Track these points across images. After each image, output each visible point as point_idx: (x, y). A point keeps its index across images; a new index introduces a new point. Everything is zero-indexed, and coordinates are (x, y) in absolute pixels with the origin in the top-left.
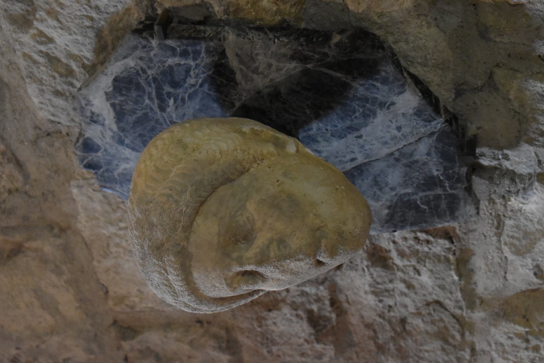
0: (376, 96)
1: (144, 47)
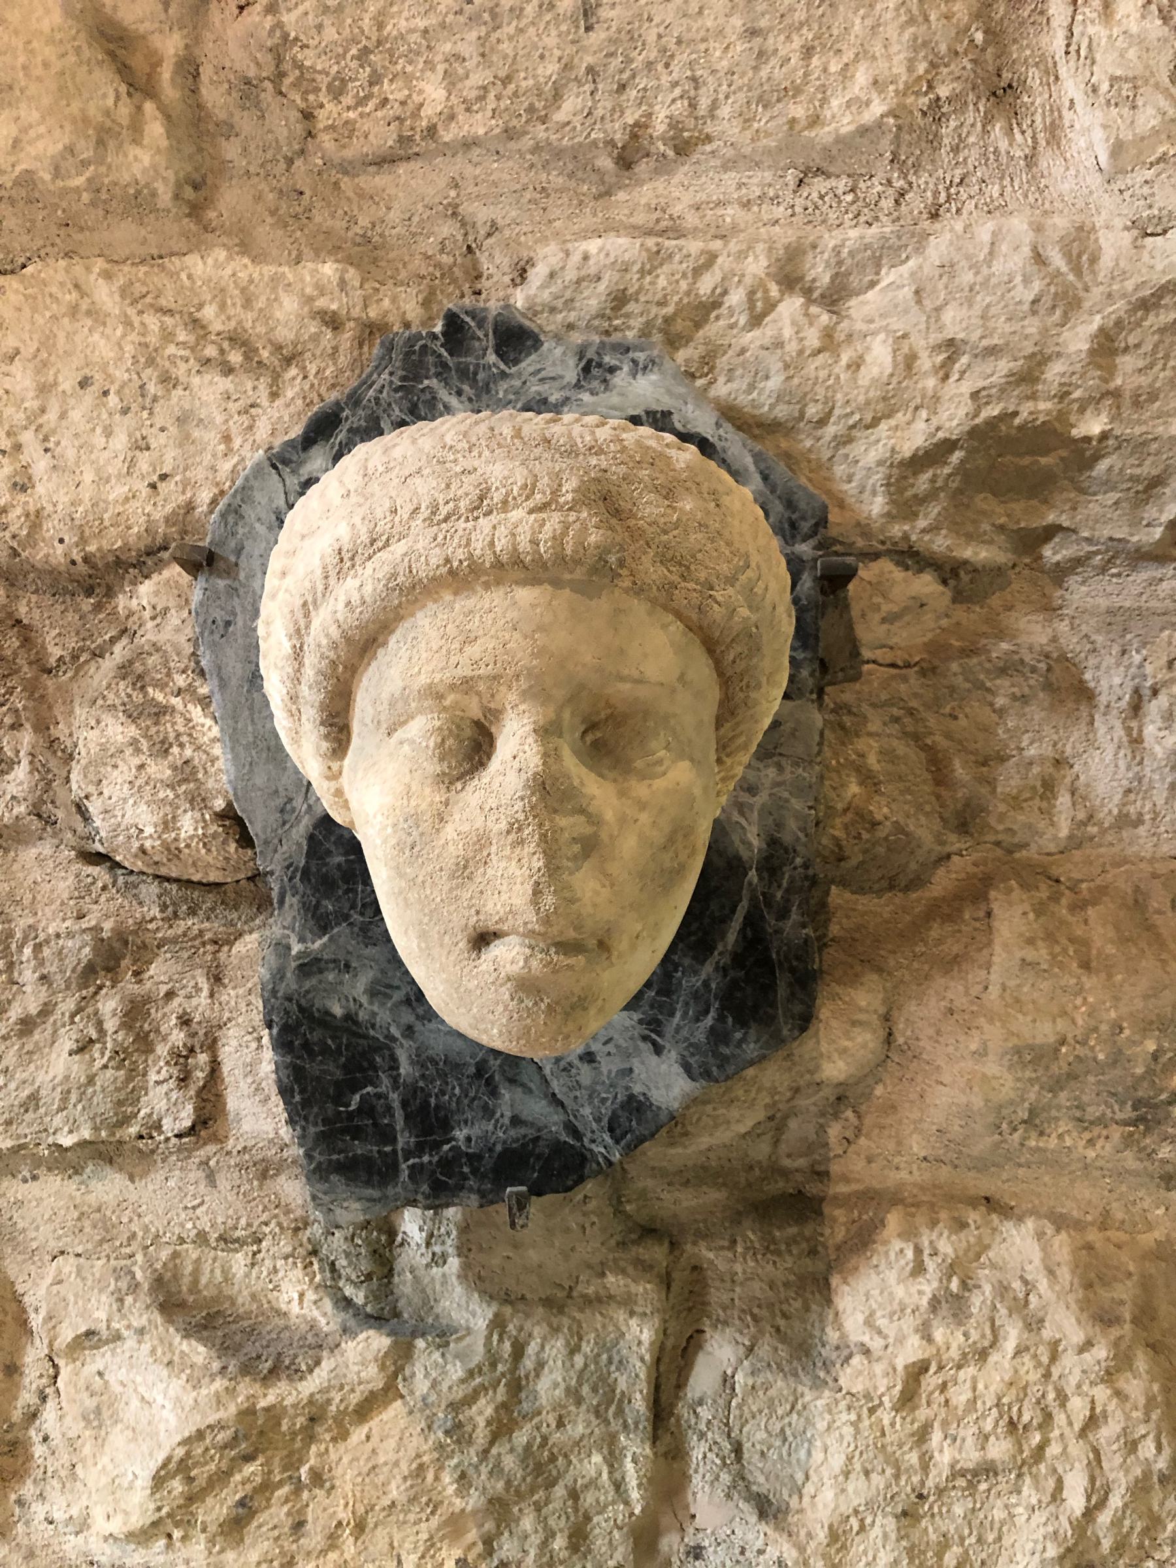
0: (678, 1015)
1: (793, 525)
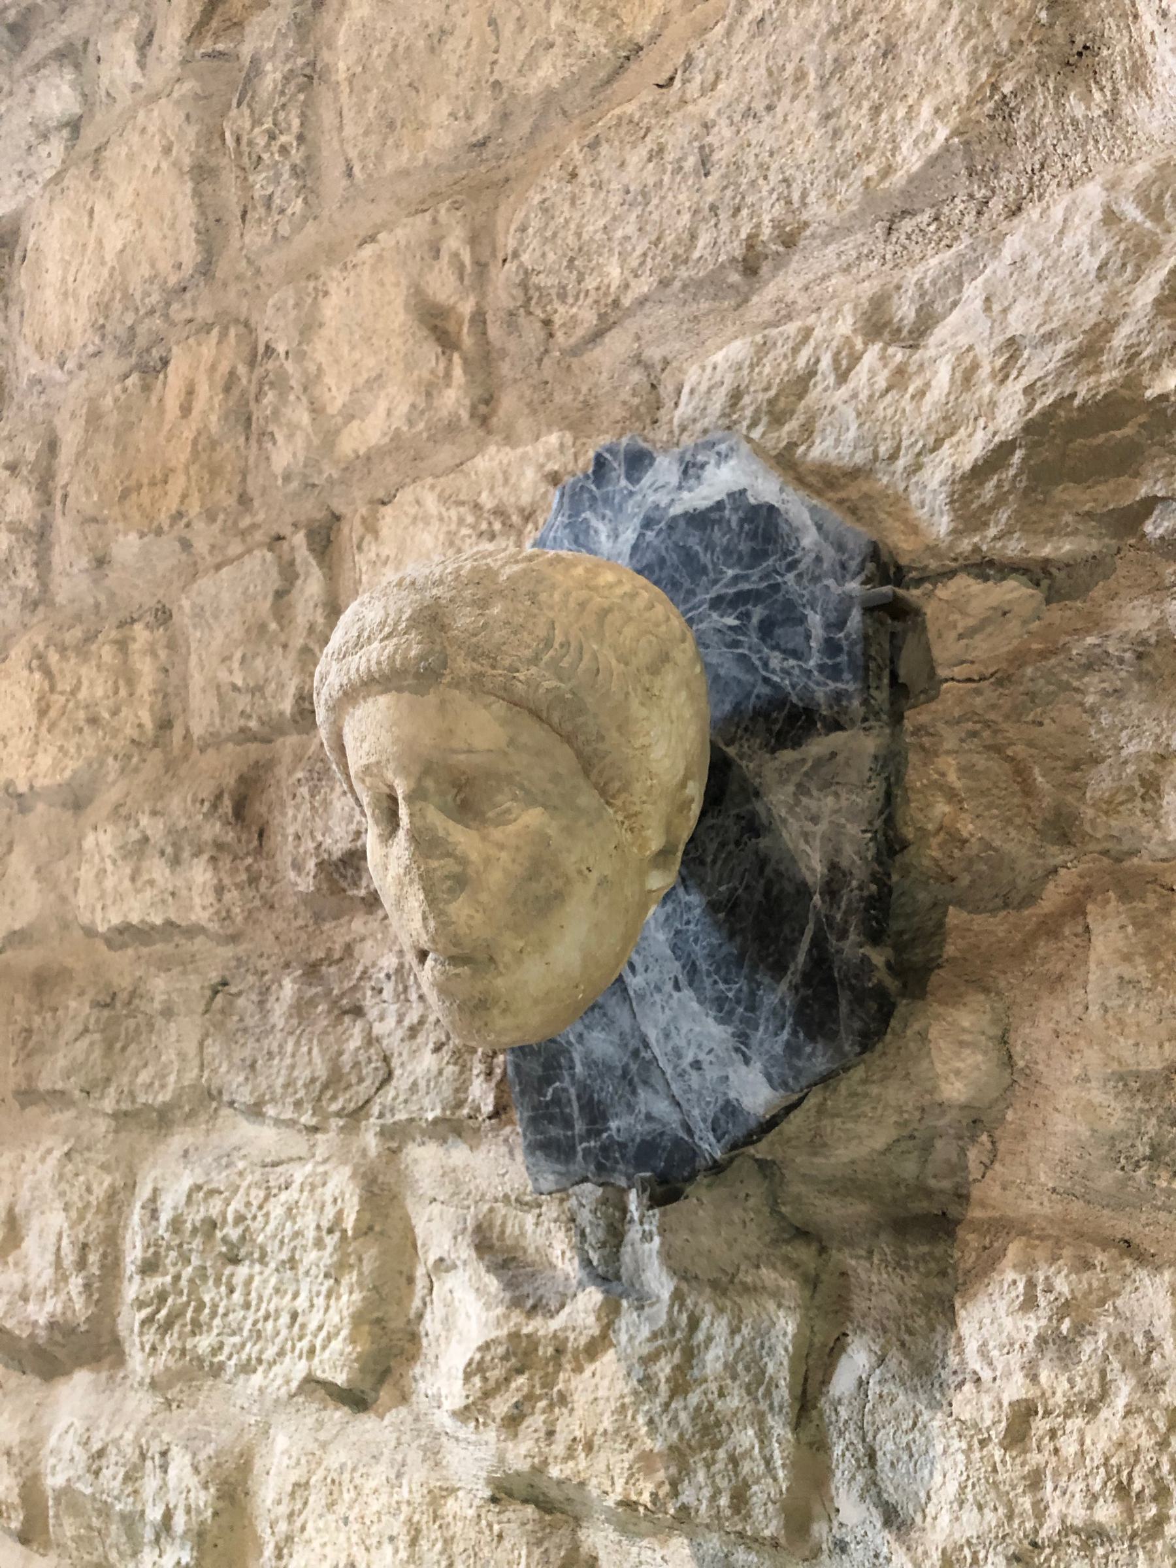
1: (843, 566)
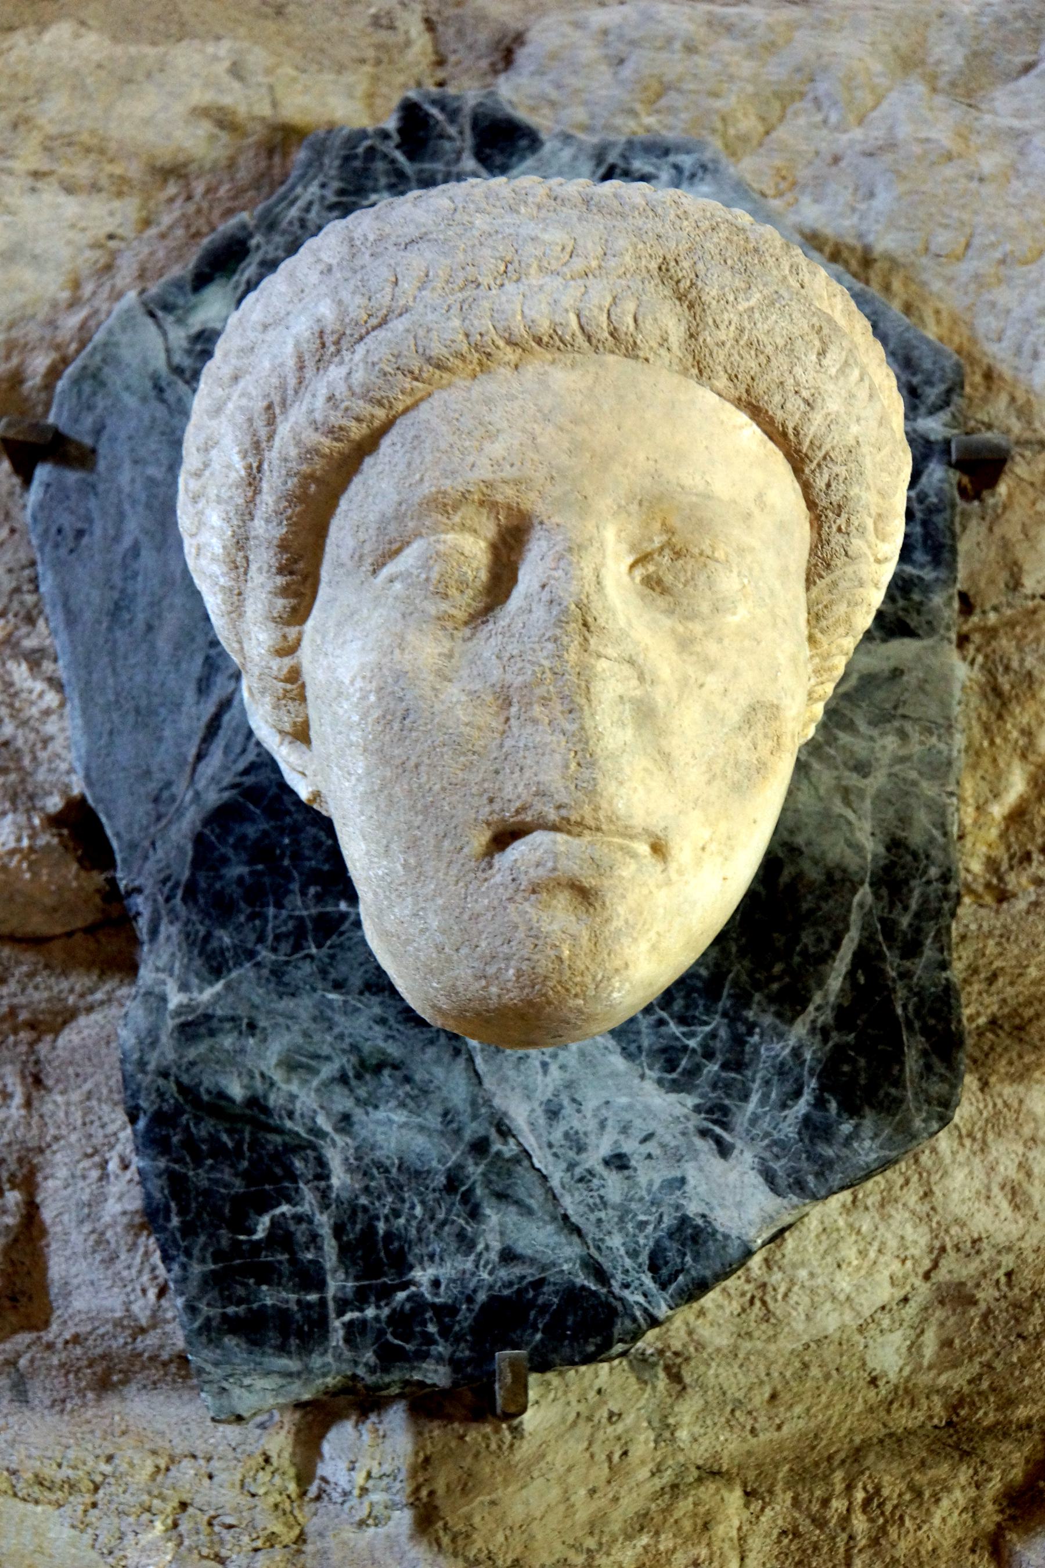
0: (755, 1098)
